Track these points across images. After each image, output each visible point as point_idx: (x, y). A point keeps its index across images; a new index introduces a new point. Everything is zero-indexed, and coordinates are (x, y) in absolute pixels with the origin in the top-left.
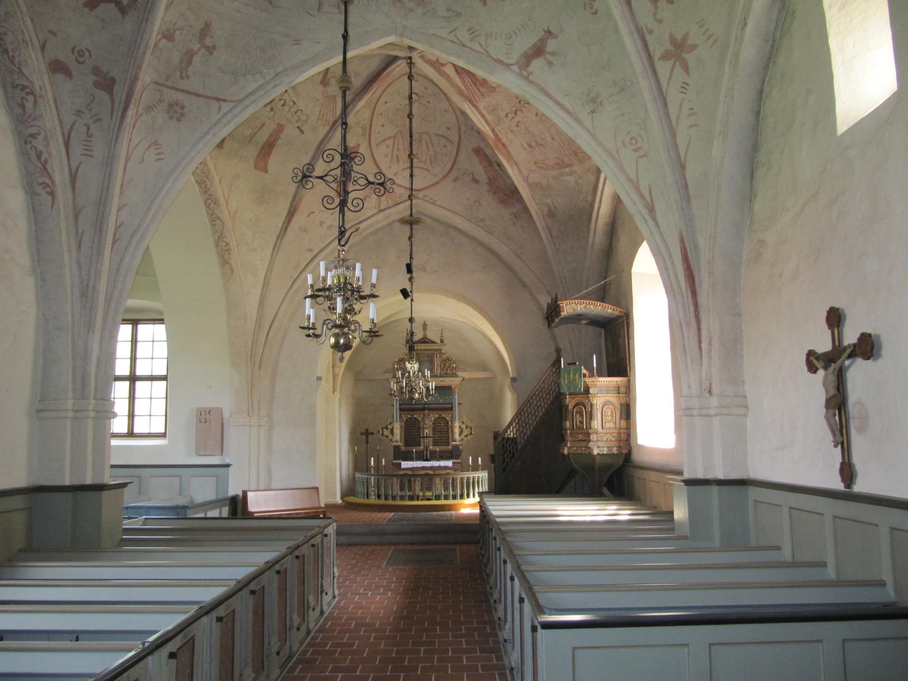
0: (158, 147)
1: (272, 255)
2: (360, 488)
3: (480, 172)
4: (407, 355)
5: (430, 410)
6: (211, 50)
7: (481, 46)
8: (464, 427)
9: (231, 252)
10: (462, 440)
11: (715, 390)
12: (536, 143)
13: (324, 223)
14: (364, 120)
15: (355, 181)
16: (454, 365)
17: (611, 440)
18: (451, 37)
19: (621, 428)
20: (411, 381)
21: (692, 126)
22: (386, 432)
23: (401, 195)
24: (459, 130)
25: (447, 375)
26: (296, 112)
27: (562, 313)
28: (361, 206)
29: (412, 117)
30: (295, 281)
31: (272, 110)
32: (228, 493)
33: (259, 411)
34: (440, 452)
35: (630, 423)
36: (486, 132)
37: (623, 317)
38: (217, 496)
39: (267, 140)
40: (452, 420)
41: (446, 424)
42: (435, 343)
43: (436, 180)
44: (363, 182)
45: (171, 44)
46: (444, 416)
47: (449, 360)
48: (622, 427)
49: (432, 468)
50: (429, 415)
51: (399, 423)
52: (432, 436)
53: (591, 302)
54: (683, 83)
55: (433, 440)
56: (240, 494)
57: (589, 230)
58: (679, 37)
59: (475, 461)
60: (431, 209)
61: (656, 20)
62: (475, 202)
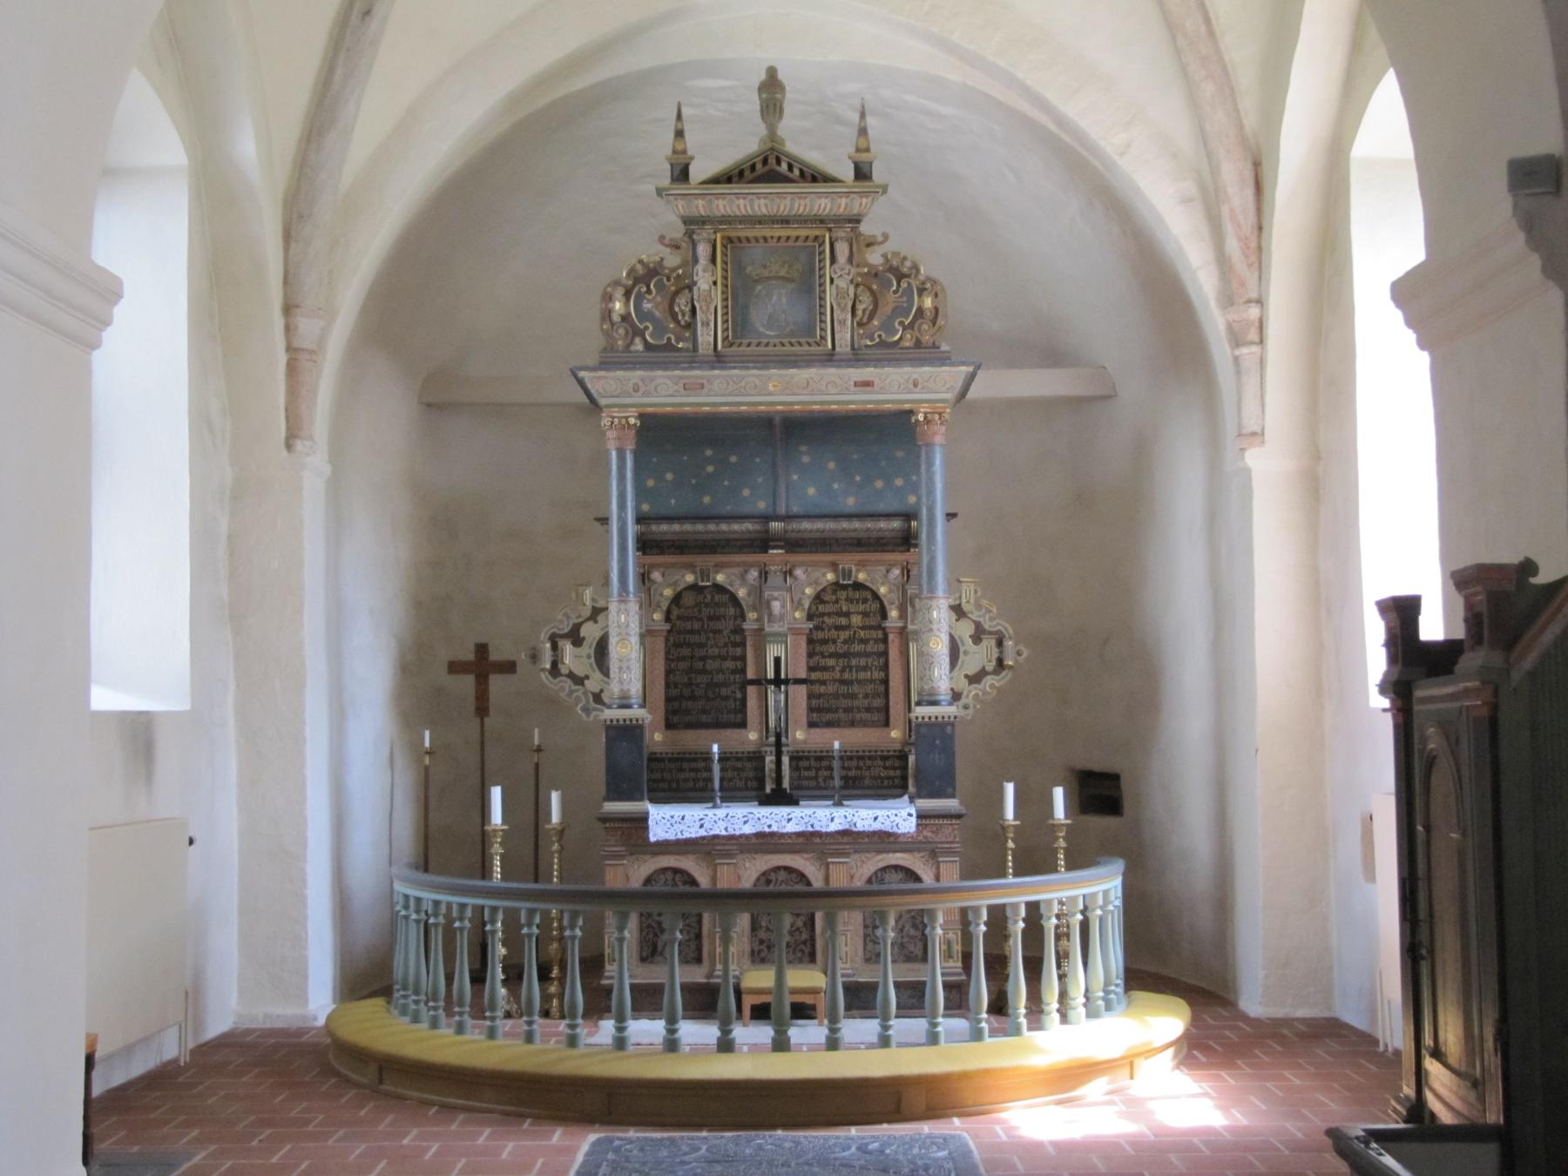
5: (795, 545)
8: (965, 630)
22: (571, 657)
25: (888, 353)
42: (828, 179)
46: (861, 577)
51: (633, 606)
55: (810, 696)
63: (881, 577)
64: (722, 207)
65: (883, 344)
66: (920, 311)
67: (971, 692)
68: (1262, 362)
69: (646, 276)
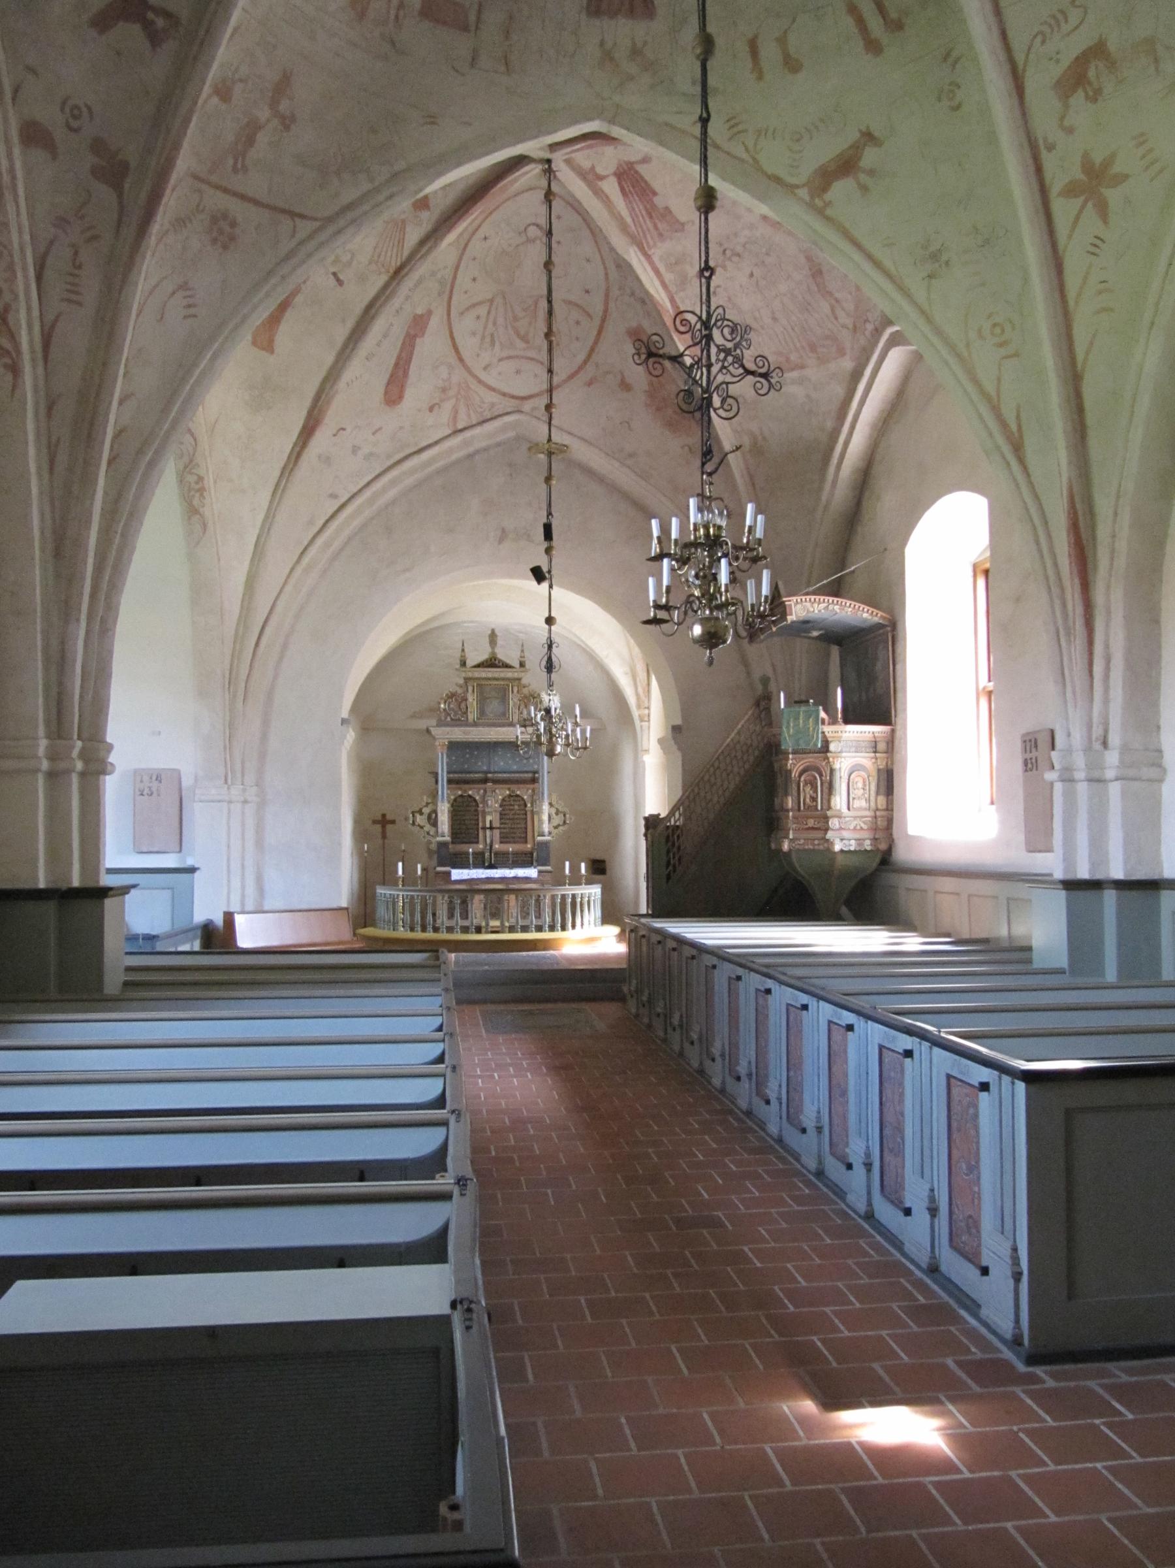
0: (188, 293)
1: (271, 502)
4: (461, 687)
5: (496, 781)
6: (287, 122)
7: (747, 150)
8: (553, 811)
9: (205, 494)
11: (1115, 739)
13: (359, 448)
14: (446, 267)
19: (877, 809)
21: (1104, 310)
22: (420, 819)
23: (493, 405)
24: (607, 295)
29: (551, 267)
30: (305, 549)
32: (192, 917)
33: (243, 775)
34: (515, 854)
35: (892, 800)
37: (887, 626)
40: (536, 797)
41: (522, 807)
42: (513, 667)
45: (224, 107)
46: (518, 793)
48: (880, 807)
49: (503, 880)
54: (1096, 237)
55: (500, 833)
56: (219, 920)
59: (575, 869)
61: (1062, 127)
63: (525, 793)
64: (476, 675)
67: (555, 832)
68: (649, 727)
69: (452, 695)
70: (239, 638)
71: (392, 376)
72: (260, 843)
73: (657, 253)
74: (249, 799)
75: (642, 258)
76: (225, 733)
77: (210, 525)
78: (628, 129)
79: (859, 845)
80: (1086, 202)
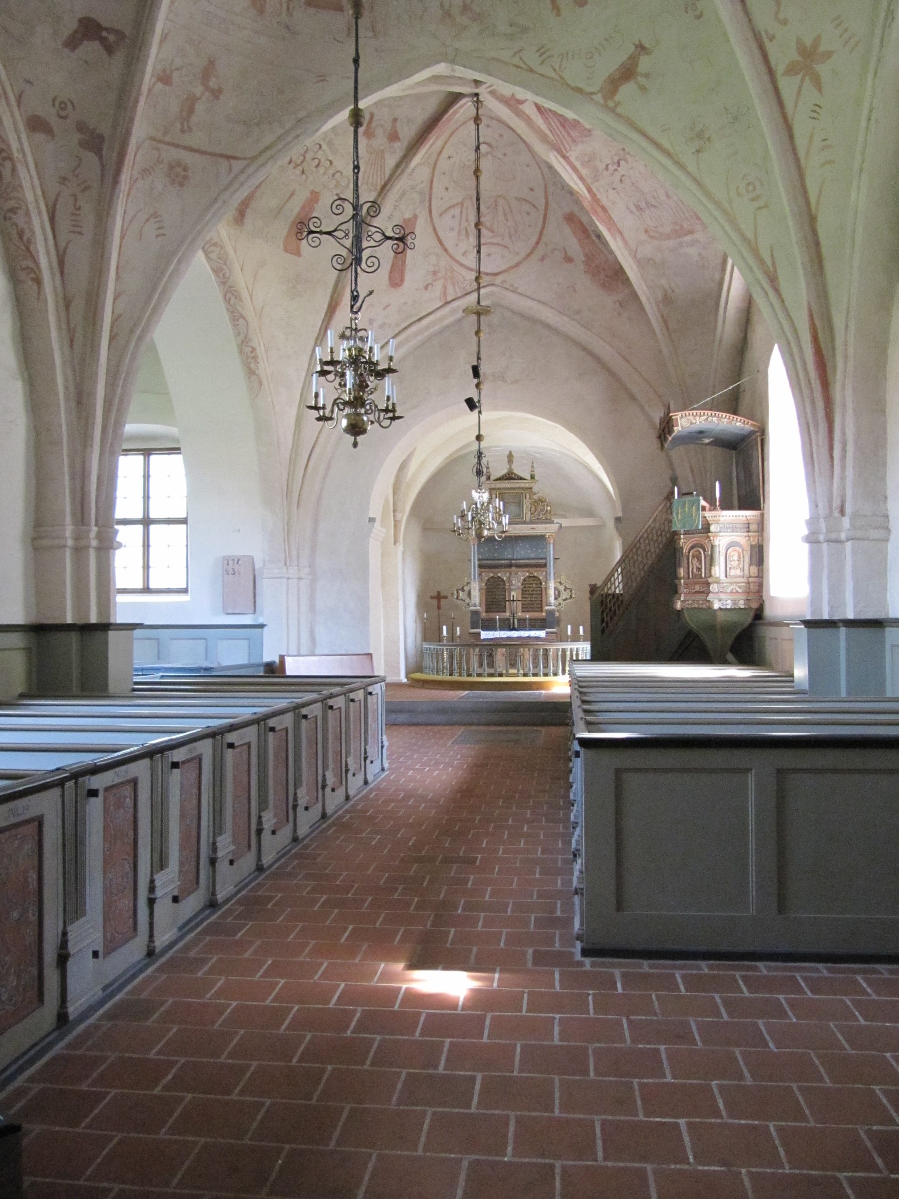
0: (158, 219)
2: (427, 662)
3: (573, 245)
5: (519, 566)
6: (216, 94)
7: (555, 70)
8: (562, 588)
10: (560, 605)
11: (848, 509)
12: (647, 203)
14: (422, 182)
15: (369, 236)
16: (549, 508)
17: (737, 592)
18: (516, 61)
20: (478, 513)
25: (539, 521)
26: (333, 175)
27: (675, 428)
28: (376, 265)
29: (479, 174)
31: (303, 172)
32: (262, 656)
34: (569, 667)
35: (762, 569)
36: (579, 191)
37: (757, 432)
38: (249, 660)
39: (299, 214)
41: (539, 585)
42: (524, 479)
43: (518, 259)
44: (378, 237)
46: (536, 574)
47: (542, 502)
48: (752, 574)
49: (519, 638)
50: (517, 573)
51: (477, 583)
52: (520, 599)
53: (713, 413)
55: (523, 605)
56: (277, 660)
57: (716, 321)
58: (808, 42)
59: (575, 631)
60: (511, 298)
62: (568, 288)
64: (498, 486)
65: (538, 519)
66: (547, 511)
70: (292, 462)
71: (392, 266)
72: (312, 608)
73: (573, 155)
74: (291, 576)
75: (562, 160)
76: (284, 529)
77: (265, 381)
78: (465, 67)
79: (734, 604)
80: (804, 76)
